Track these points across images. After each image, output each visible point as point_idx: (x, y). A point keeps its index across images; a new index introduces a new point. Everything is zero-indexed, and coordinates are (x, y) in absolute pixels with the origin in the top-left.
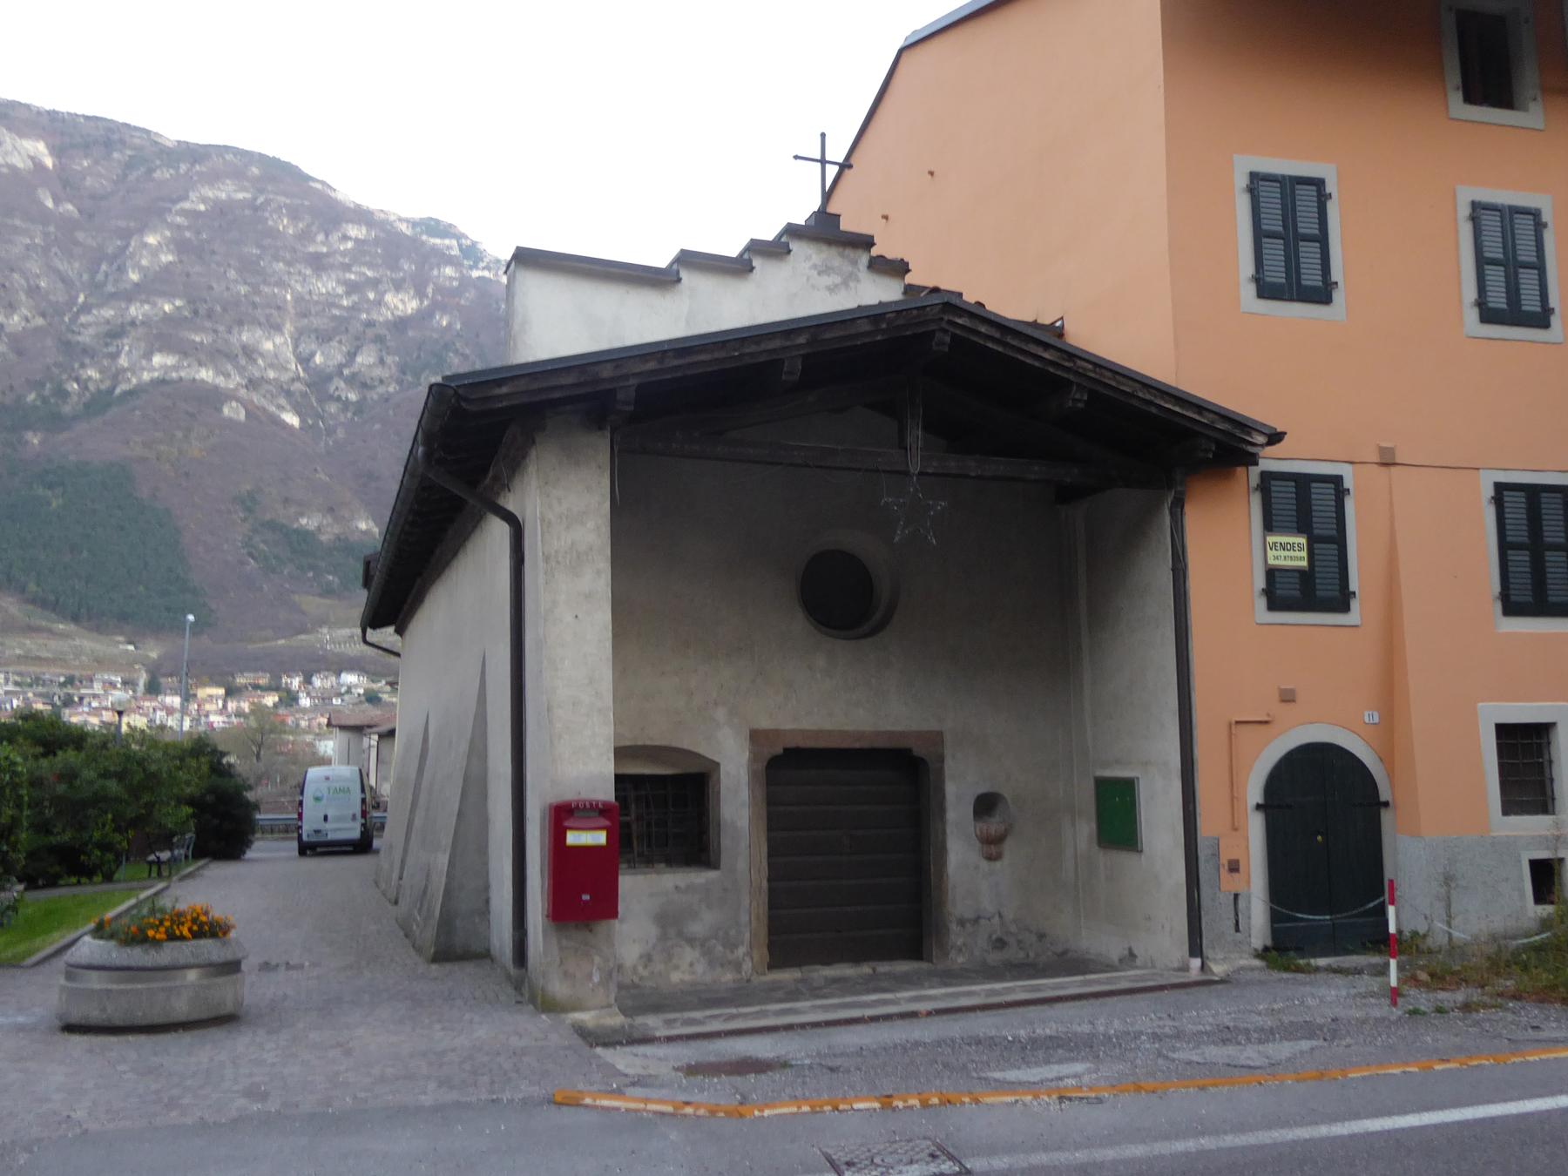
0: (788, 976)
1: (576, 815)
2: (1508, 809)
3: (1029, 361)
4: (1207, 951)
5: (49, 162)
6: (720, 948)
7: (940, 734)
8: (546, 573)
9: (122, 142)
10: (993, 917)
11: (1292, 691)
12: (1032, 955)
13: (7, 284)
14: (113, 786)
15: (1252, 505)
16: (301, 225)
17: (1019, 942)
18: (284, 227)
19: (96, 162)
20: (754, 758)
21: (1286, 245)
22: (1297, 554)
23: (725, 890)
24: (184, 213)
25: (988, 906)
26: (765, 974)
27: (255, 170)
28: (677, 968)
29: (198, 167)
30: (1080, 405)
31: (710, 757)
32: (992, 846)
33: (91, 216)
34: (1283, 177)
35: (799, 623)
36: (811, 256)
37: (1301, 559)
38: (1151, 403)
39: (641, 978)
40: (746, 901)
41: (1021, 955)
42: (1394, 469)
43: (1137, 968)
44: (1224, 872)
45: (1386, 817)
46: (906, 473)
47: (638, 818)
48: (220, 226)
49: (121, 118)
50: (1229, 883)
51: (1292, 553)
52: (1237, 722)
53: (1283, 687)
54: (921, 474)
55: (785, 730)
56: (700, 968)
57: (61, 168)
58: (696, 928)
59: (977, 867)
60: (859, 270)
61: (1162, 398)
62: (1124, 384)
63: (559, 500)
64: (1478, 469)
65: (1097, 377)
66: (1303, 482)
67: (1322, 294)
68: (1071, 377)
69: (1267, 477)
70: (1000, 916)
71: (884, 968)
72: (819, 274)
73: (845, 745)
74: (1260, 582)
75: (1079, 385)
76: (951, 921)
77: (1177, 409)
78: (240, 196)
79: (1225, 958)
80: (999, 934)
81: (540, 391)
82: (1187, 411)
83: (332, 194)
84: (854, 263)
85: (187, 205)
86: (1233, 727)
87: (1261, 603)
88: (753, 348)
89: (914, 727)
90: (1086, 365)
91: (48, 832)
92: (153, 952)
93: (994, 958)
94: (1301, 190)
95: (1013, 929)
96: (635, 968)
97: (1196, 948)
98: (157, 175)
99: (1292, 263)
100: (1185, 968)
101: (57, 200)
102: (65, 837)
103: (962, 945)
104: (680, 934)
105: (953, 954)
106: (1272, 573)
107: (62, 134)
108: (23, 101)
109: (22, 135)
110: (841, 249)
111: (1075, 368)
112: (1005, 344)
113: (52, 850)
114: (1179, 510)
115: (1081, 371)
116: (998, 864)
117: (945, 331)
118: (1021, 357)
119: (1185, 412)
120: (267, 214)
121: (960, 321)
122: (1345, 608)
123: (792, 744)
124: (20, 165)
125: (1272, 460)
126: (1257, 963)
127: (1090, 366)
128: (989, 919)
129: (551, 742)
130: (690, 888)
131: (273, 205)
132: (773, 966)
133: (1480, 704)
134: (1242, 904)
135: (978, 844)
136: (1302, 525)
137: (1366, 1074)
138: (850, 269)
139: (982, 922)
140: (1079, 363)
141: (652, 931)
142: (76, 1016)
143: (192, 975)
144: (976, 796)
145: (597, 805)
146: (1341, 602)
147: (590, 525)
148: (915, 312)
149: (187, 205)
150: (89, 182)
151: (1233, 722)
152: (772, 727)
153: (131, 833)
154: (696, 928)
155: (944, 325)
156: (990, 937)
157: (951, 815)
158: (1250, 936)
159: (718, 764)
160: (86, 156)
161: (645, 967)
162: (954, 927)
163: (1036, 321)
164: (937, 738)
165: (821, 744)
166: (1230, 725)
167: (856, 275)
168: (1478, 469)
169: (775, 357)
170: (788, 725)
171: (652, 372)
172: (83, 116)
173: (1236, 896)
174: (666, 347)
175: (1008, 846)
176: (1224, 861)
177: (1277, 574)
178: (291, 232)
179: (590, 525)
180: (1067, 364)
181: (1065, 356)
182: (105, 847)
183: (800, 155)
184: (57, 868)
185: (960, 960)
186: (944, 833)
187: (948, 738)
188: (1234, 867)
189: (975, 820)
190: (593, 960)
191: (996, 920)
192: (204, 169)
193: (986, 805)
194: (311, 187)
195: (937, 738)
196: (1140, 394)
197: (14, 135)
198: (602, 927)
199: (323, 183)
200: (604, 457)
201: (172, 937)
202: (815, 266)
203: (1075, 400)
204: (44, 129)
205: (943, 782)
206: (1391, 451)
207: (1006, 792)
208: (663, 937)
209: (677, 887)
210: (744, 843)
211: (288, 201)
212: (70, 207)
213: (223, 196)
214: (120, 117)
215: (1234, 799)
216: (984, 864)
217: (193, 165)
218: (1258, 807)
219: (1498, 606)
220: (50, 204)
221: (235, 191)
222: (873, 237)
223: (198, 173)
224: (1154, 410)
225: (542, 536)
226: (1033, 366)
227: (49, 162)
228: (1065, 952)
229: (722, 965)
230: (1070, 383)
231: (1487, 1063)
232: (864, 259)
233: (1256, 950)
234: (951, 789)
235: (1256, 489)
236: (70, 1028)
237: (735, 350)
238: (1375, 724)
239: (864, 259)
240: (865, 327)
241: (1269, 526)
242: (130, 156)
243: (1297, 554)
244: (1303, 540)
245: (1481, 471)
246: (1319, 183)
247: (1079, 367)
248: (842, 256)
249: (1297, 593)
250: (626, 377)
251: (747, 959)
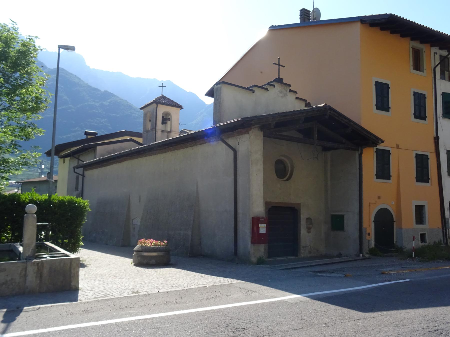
32: (309, 230)
43: (342, 257)
44: (367, 235)
64: (413, 150)
70: (310, 246)
72: (280, 93)
86: (370, 204)
90: (352, 123)
99: (420, 113)
100: (359, 256)
139: (307, 247)
166: (369, 203)
168: (413, 150)
176: (367, 233)
188: (369, 234)
191: (309, 247)
193: (309, 220)
202: (279, 91)
218: (373, 221)
234: (302, 216)
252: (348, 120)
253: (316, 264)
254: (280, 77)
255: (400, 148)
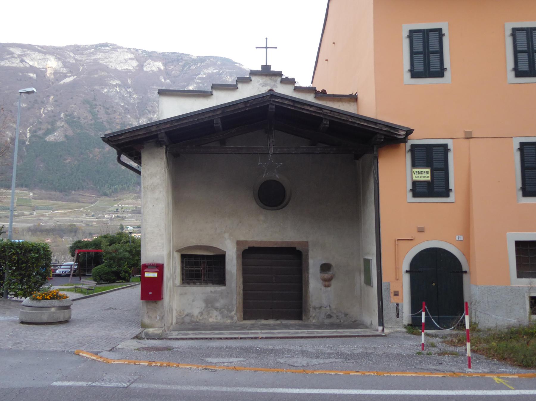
0: (248, 322)
1: (148, 267)
2: (520, 276)
3: (305, 112)
4: (385, 325)
5: (162, 68)
6: (226, 312)
7: (307, 242)
8: (144, 193)
9: (182, 59)
10: (327, 307)
11: (423, 228)
12: (342, 321)
13: (153, 106)
14: (127, 254)
15: (407, 158)
16: (233, 78)
17: (337, 316)
18: (228, 79)
19: (175, 66)
20: (238, 250)
21: (425, 57)
22: (426, 175)
23: (228, 293)
24: (199, 78)
25: (325, 303)
26: (241, 321)
27: (219, 63)
28: (211, 317)
29: (203, 64)
30: (327, 126)
31: (223, 249)
32: (327, 282)
33: (174, 83)
34: (424, 30)
35: (254, 205)
36: (259, 81)
37: (427, 177)
38: (354, 123)
39: (199, 320)
40: (235, 297)
41: (338, 321)
42: (470, 140)
43: (307, 327)
44: (392, 295)
45: (465, 277)
46: (269, 154)
47: (204, 269)
48: (210, 81)
49: (181, 52)
50: (394, 300)
51: (423, 175)
52: (398, 240)
53: (418, 226)
54: (273, 154)
55: (249, 241)
56: (219, 318)
57: (166, 69)
58: (218, 305)
59: (321, 289)
60: (277, 84)
61: (359, 121)
62: (342, 117)
63: (148, 170)
64: (512, 137)
65: (332, 115)
66: (429, 148)
67: (440, 73)
68: (322, 116)
69: (413, 147)
70: (330, 307)
71: (285, 322)
72: (262, 86)
73: (271, 246)
74: (410, 186)
75: (325, 119)
76: (311, 308)
77: (366, 124)
78: (215, 71)
79: (392, 327)
80: (329, 313)
81: (134, 136)
82: (370, 124)
83: (242, 67)
84: (276, 81)
85: (200, 76)
86: (396, 241)
87: (410, 194)
88: (202, 117)
89: (297, 240)
90: (326, 111)
91: (112, 267)
92: (38, 302)
93: (327, 321)
94: (431, 34)
95: (335, 312)
96: (197, 316)
97: (381, 323)
98: (192, 68)
99: (427, 63)
101: (165, 80)
102: (115, 269)
103: (313, 316)
104: (212, 306)
105: (311, 319)
106: (414, 183)
107: (166, 59)
108: (155, 51)
109: (155, 61)
110: (270, 77)
111: (323, 113)
112: (295, 107)
113: (113, 272)
114: (376, 161)
115: (325, 113)
116: (329, 289)
117: (272, 104)
118: (301, 111)
119: (369, 125)
120: (223, 76)
121: (277, 100)
122: (448, 196)
123: (252, 245)
124: (155, 70)
125: (413, 140)
126: (405, 330)
127: (329, 112)
128: (325, 308)
129: (145, 244)
130: (215, 292)
131: (225, 73)
132: (244, 319)
133: (508, 233)
134: (400, 307)
135: (321, 281)
136: (428, 164)
137: (414, 375)
138: (274, 83)
139: (323, 308)
140: (324, 111)
141: (203, 305)
142: (24, 319)
143: (53, 309)
144: (321, 264)
145: (154, 264)
146: (446, 192)
147: (158, 177)
148: (260, 99)
149: (200, 76)
150: (173, 72)
151: (396, 240)
152: (245, 240)
153: (133, 268)
154: (218, 305)
155: (271, 102)
156: (326, 314)
157: (311, 271)
158: (403, 320)
159: (226, 252)
160: (172, 65)
161: (201, 316)
162: (311, 309)
163: (352, 94)
164: (306, 244)
165: (262, 246)
167: (276, 85)
168: (512, 137)
169: (210, 119)
170: (250, 239)
171: (168, 128)
172: (171, 53)
173: (398, 305)
174: (173, 119)
175: (333, 282)
177: (417, 183)
178: (230, 80)
179: (158, 177)
180: (319, 112)
181: (319, 109)
182: (126, 272)
183: (258, 47)
184: (114, 278)
185: (314, 321)
186: (308, 277)
187: (310, 244)
188: (396, 294)
189: (321, 273)
190: (157, 313)
191: (328, 308)
192: (204, 64)
193: (325, 268)
194: (236, 66)
195: (306, 244)
196: (350, 120)
197: (153, 61)
198: (160, 302)
199: (239, 64)
200: (164, 156)
201: (43, 298)
202: (261, 84)
203: (324, 124)
204: (161, 58)
205: (308, 259)
206: (470, 133)
207: (332, 263)
208: (207, 307)
209: (211, 291)
210: (235, 277)
211: (229, 71)
212: (168, 81)
213: (210, 72)
214: (180, 51)
215: (397, 269)
216: (324, 288)
217: (201, 63)
218: (407, 272)
219: (520, 193)
220: (163, 80)
221: (214, 70)
222: (281, 72)
223: (203, 66)
224: (356, 125)
225: (143, 181)
226: (307, 113)
227: (162, 68)
228: (355, 321)
229: (227, 317)
230: (322, 119)
231: (373, 374)
232: (279, 79)
233: (405, 325)
234: (311, 262)
235: (409, 151)
236: (22, 322)
237: (196, 118)
238: (461, 240)
239: (279, 79)
240: (242, 106)
241: (414, 165)
242: (184, 63)
243: (426, 175)
244: (428, 170)
245: (513, 138)
246: (440, 30)
247: (324, 112)
248: (270, 79)
249: (426, 190)
250: (160, 130)
251: (235, 316)
252: (315, 106)
253: (264, 336)
254: (268, 65)
255: (473, 138)
